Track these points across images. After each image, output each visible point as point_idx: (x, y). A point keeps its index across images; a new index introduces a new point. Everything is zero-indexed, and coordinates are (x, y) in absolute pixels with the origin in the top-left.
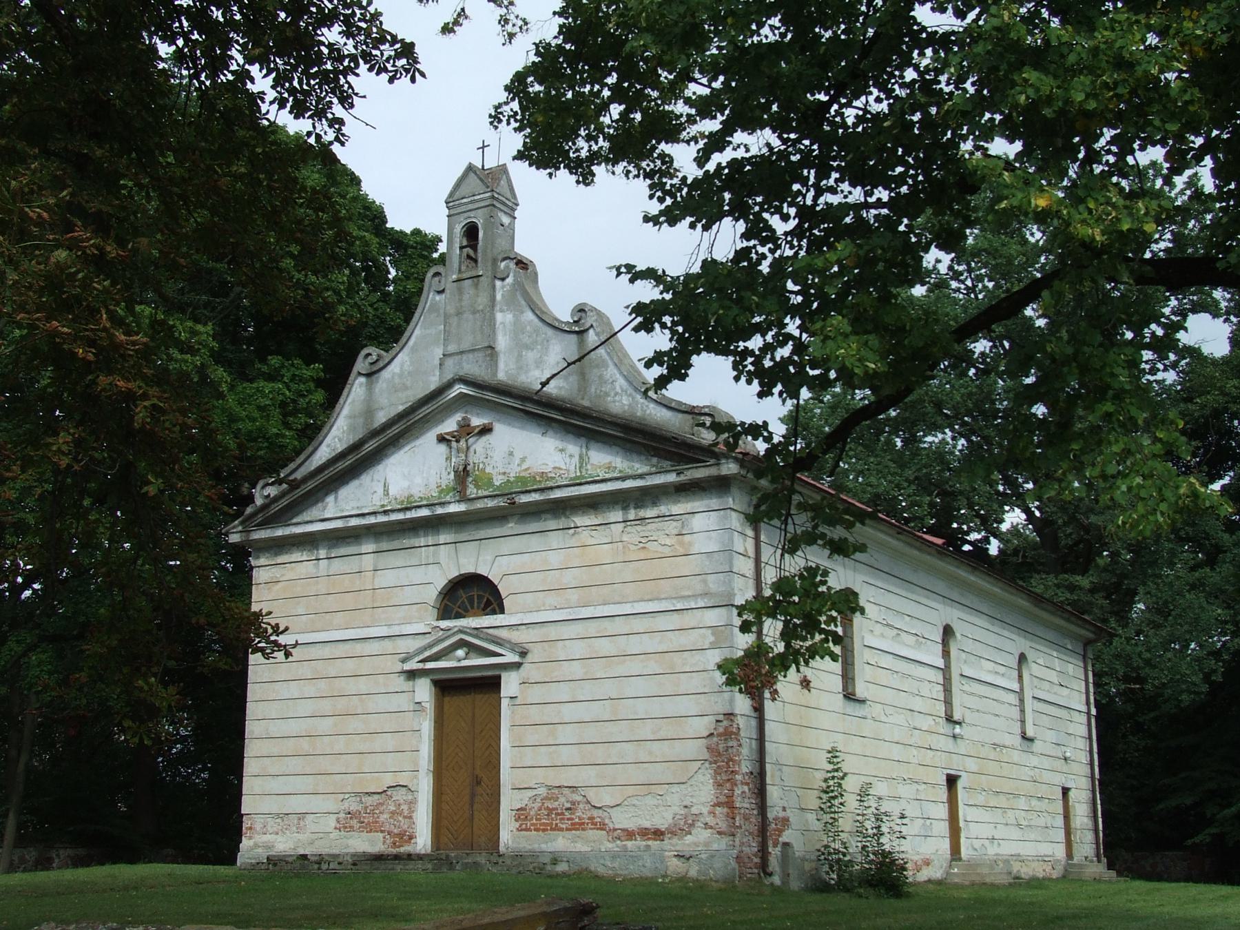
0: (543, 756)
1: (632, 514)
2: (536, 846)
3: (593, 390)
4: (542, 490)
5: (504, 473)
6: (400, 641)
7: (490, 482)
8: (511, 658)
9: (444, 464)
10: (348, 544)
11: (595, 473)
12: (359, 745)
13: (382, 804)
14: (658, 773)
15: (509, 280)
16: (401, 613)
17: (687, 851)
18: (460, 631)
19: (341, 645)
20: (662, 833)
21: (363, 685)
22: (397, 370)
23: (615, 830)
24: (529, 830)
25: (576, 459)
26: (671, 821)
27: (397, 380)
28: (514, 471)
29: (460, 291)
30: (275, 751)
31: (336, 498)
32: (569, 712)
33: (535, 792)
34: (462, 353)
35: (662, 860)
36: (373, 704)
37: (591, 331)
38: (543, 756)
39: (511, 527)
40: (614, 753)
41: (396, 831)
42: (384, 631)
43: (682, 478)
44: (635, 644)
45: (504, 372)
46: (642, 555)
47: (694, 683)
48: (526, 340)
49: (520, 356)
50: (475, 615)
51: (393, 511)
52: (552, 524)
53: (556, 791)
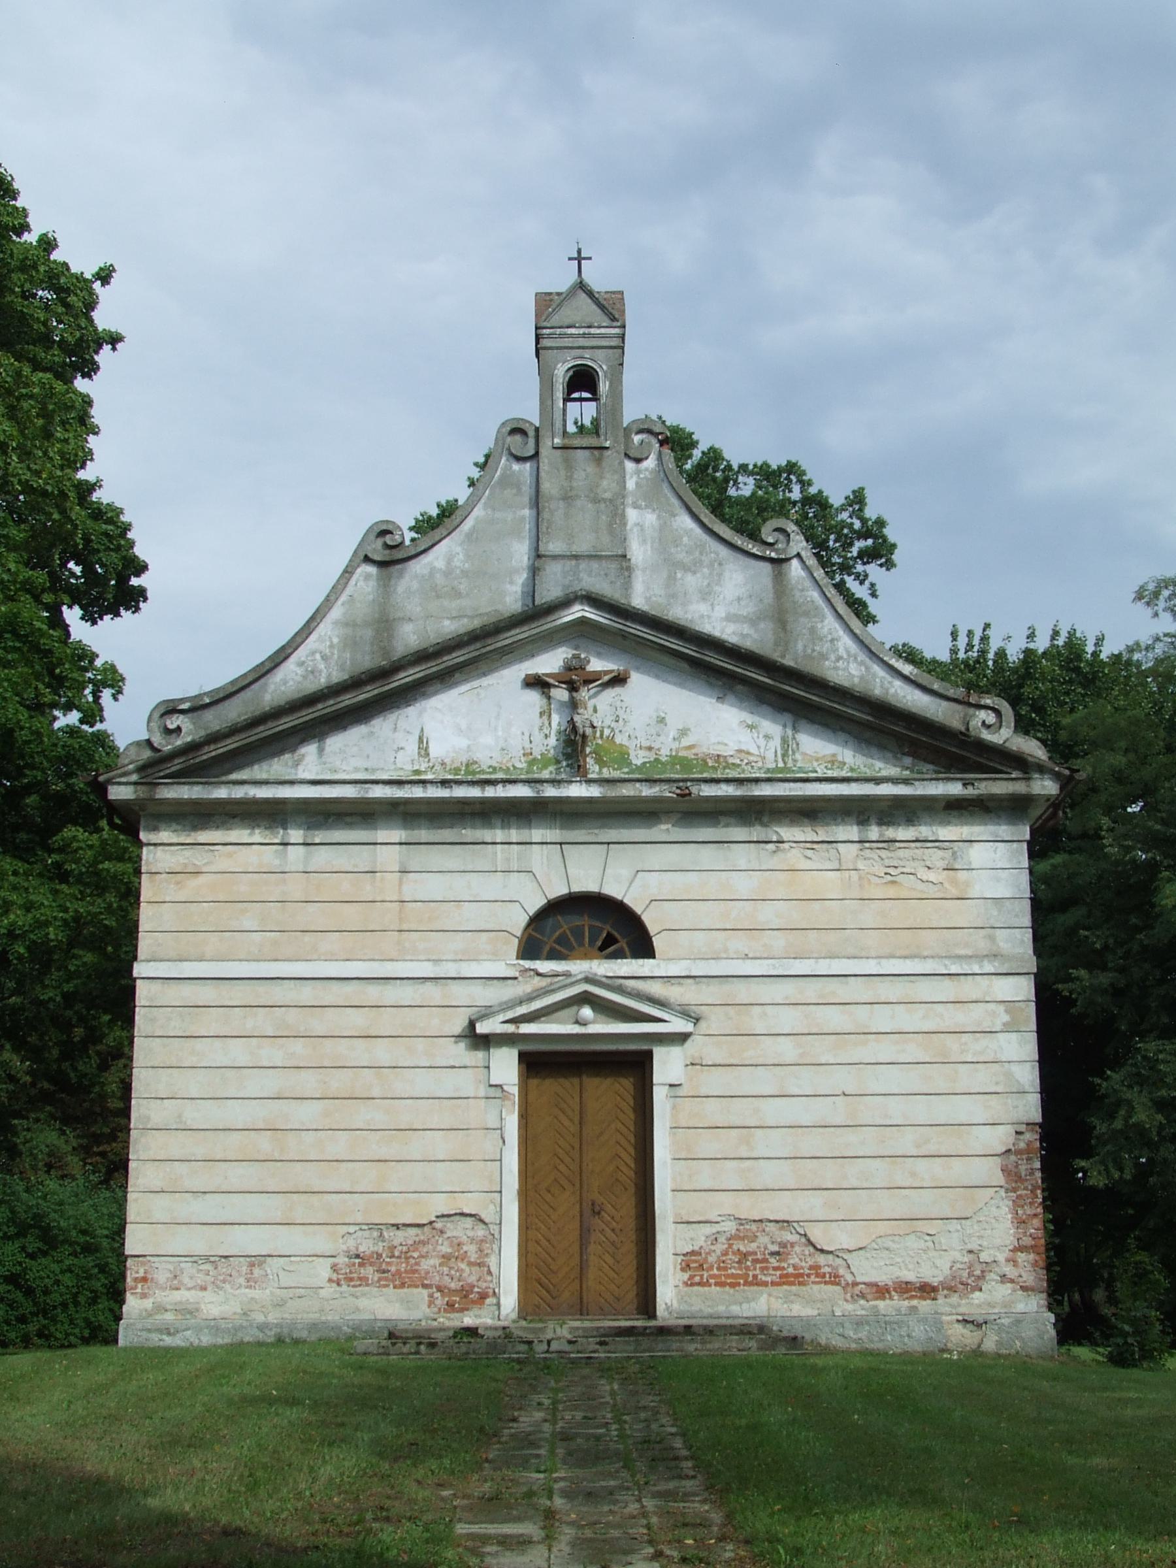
0: (730, 1174)
1: (874, 832)
2: (721, 1309)
3: (800, 646)
4: (740, 782)
5: (650, 749)
6: (456, 988)
7: (623, 758)
8: (677, 1025)
9: (537, 721)
10: (350, 826)
11: (808, 766)
12: (376, 1147)
13: (423, 1243)
14: (923, 1203)
15: (650, 463)
16: (457, 943)
17: (977, 1314)
18: (587, 980)
19: (335, 985)
20: (934, 1289)
21: (382, 1052)
22: (440, 564)
23: (855, 1284)
24: (708, 1284)
25: (776, 743)
26: (947, 1272)
27: (439, 579)
28: (666, 747)
29: (569, 466)
30: (200, 1152)
31: (321, 751)
32: (773, 1111)
33: (717, 1228)
34: (576, 557)
35: (939, 1326)
36: (401, 1084)
37: (795, 563)
38: (730, 1174)
39: (664, 830)
40: (853, 1173)
41: (453, 1285)
42: (427, 970)
43: (970, 791)
44: (882, 1019)
45: (642, 595)
46: (892, 892)
47: (983, 1078)
48: (681, 556)
49: (671, 578)
50: (586, 956)
51: (459, 783)
52: (738, 833)
53: (754, 1227)
